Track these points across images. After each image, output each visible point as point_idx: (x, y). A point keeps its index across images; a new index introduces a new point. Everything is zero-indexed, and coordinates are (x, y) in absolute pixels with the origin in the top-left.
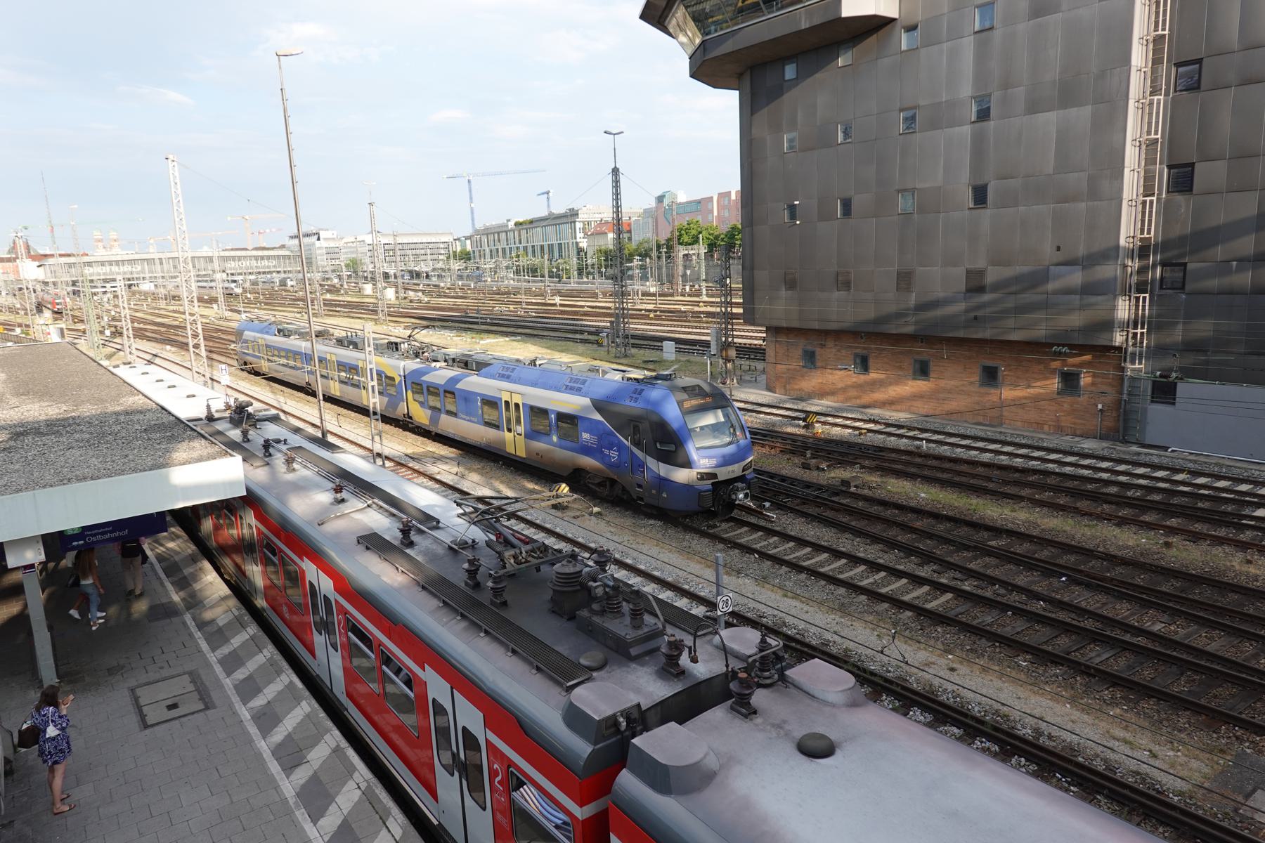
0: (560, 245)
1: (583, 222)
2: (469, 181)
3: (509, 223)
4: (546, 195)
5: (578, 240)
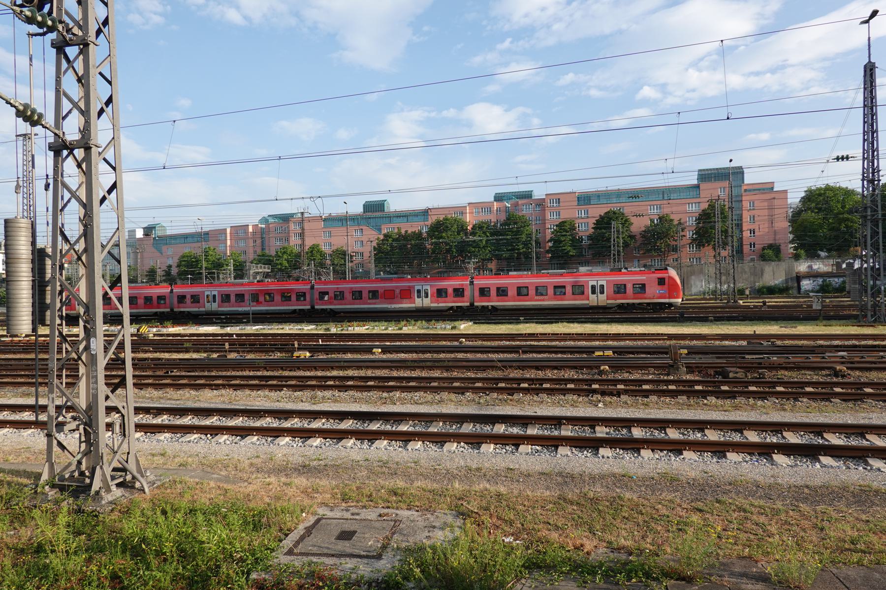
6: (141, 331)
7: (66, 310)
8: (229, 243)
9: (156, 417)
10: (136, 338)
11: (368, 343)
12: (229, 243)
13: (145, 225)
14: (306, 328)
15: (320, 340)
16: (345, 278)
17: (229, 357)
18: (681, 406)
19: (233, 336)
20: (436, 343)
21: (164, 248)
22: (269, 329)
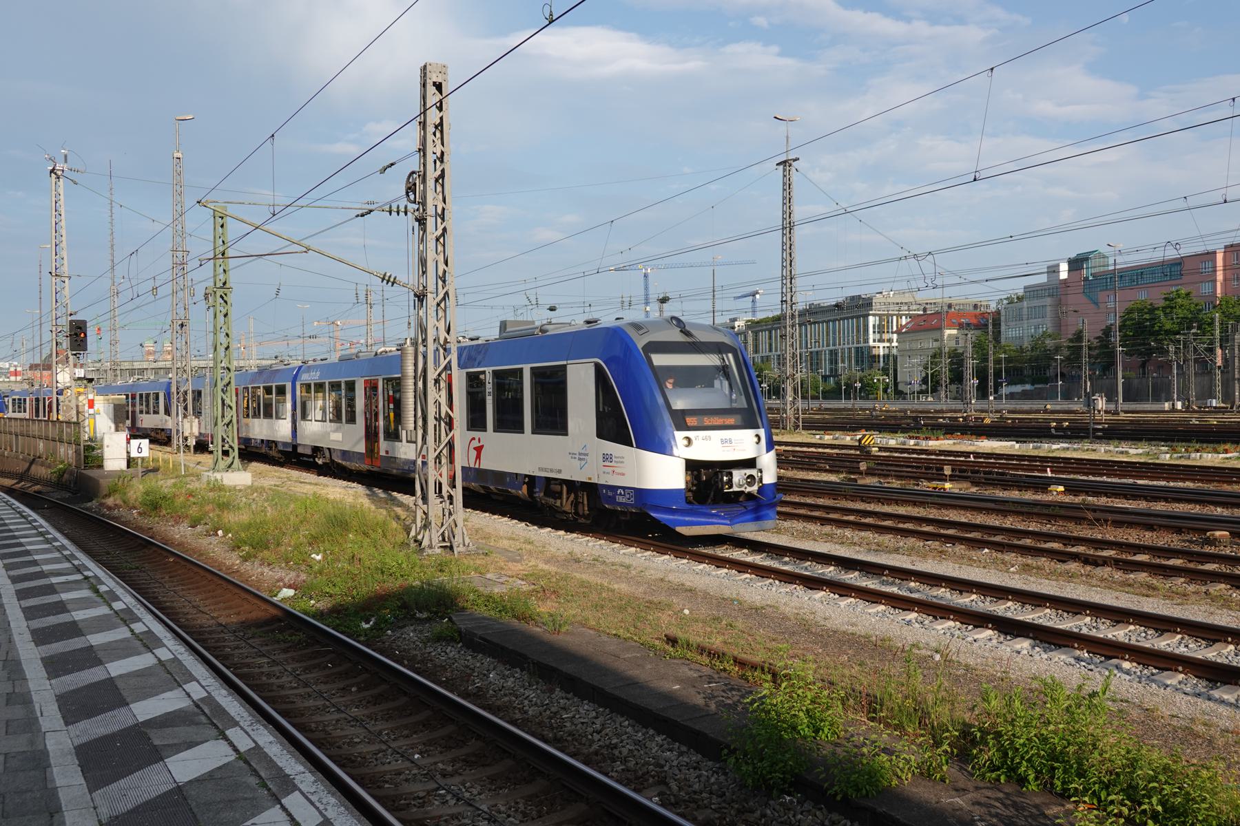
0: (833, 353)
1: (880, 316)
2: (646, 276)
3: (737, 324)
4: (751, 297)
5: (871, 343)
6: (863, 442)
7: (272, 399)
8: (1220, 276)
9: (1160, 635)
10: (858, 453)
11: (1189, 484)
12: (1220, 276)
13: (1073, 255)
14: (1132, 451)
15: (1048, 469)
16: (399, 378)
17: (860, 482)
18: (1108, 584)
19: (970, 457)
20: (1155, 483)
21: (1101, 296)
22: (1075, 450)
